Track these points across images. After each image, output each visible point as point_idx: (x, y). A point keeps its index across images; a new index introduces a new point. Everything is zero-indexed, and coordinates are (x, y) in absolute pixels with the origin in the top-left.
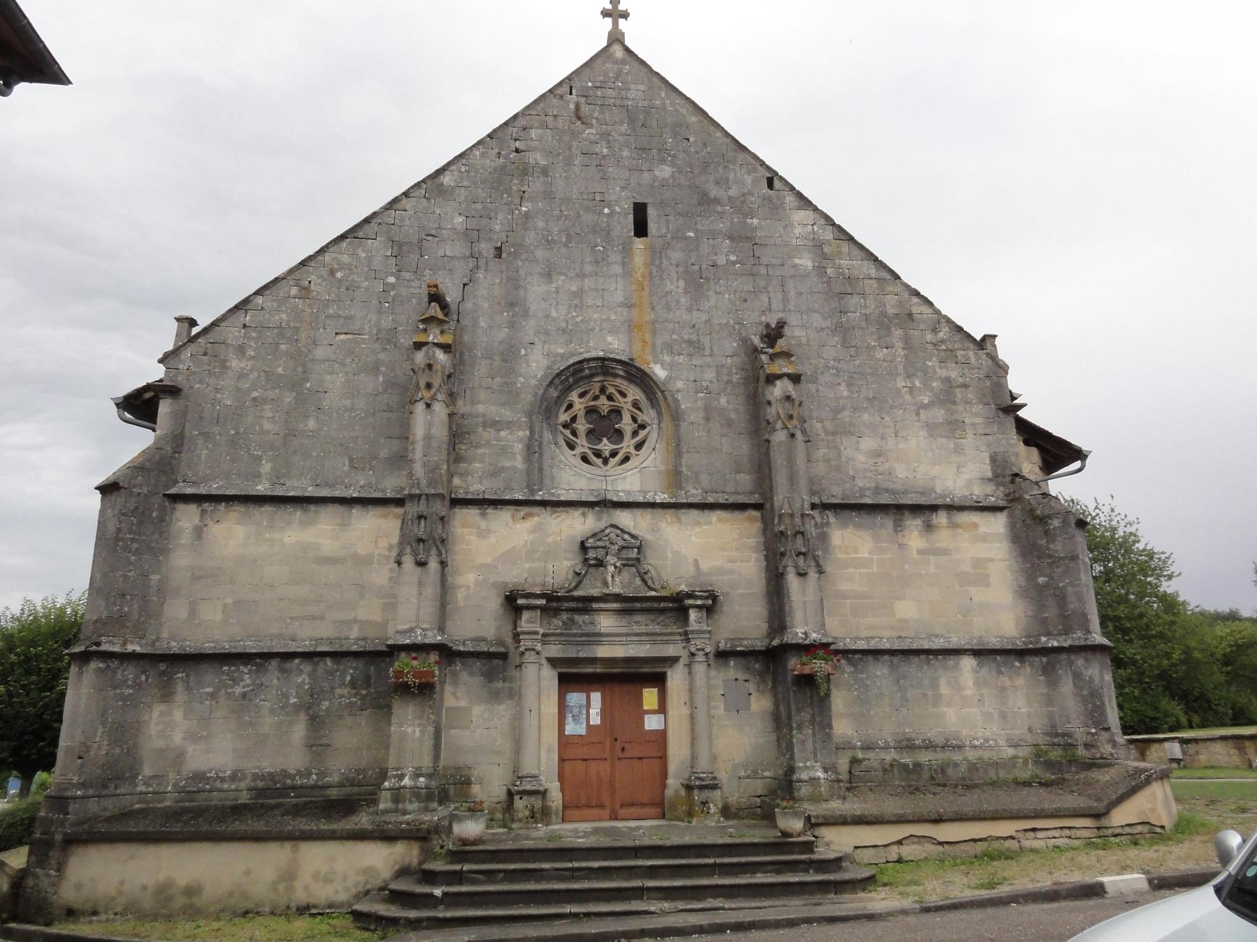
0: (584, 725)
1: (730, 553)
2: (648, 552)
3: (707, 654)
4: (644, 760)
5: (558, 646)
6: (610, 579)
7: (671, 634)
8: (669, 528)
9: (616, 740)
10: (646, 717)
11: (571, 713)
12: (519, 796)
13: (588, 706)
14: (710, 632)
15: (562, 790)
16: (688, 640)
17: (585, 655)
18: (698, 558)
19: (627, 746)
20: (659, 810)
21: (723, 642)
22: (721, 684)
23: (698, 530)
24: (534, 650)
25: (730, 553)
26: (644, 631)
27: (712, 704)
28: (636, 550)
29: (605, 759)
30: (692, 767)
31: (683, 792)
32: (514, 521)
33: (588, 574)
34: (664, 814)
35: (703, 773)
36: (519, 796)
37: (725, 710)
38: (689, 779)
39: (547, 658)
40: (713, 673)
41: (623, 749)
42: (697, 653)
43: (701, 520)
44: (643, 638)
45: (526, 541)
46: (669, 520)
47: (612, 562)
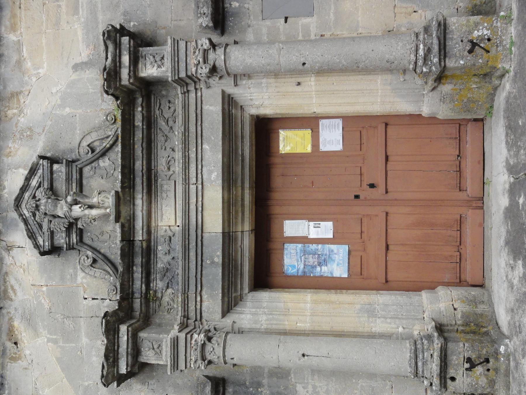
0: (334, 247)
1: (64, 9)
2: (63, 146)
3: (214, 46)
4: (388, 154)
5: (205, 297)
6: (94, 212)
7: (186, 107)
8: (28, 111)
9: (357, 197)
10: (323, 148)
11: (313, 267)
12: (449, 382)
13: (304, 240)
14: (176, 43)
15: (432, 287)
16: (194, 79)
17: (219, 253)
18: (72, 63)
19: (367, 180)
20: (470, 131)
21: (201, 20)
22: (268, 23)
23: (29, 64)
24: (203, 345)
25: (64, 9)
26: (180, 154)
27: (300, 38)
28: (56, 167)
29: (387, 214)
30: (405, 71)
31: (446, 88)
32: (19, 358)
33: (95, 245)
34: (476, 120)
35: (417, 50)
36: (449, 382)
37: (311, 14)
38: (425, 75)
39: (223, 316)
40: (250, 36)
41: (372, 186)
42: (211, 62)
43: (15, 58)
44: (193, 155)
45: (49, 340)
46: (15, 111)
47: (65, 208)
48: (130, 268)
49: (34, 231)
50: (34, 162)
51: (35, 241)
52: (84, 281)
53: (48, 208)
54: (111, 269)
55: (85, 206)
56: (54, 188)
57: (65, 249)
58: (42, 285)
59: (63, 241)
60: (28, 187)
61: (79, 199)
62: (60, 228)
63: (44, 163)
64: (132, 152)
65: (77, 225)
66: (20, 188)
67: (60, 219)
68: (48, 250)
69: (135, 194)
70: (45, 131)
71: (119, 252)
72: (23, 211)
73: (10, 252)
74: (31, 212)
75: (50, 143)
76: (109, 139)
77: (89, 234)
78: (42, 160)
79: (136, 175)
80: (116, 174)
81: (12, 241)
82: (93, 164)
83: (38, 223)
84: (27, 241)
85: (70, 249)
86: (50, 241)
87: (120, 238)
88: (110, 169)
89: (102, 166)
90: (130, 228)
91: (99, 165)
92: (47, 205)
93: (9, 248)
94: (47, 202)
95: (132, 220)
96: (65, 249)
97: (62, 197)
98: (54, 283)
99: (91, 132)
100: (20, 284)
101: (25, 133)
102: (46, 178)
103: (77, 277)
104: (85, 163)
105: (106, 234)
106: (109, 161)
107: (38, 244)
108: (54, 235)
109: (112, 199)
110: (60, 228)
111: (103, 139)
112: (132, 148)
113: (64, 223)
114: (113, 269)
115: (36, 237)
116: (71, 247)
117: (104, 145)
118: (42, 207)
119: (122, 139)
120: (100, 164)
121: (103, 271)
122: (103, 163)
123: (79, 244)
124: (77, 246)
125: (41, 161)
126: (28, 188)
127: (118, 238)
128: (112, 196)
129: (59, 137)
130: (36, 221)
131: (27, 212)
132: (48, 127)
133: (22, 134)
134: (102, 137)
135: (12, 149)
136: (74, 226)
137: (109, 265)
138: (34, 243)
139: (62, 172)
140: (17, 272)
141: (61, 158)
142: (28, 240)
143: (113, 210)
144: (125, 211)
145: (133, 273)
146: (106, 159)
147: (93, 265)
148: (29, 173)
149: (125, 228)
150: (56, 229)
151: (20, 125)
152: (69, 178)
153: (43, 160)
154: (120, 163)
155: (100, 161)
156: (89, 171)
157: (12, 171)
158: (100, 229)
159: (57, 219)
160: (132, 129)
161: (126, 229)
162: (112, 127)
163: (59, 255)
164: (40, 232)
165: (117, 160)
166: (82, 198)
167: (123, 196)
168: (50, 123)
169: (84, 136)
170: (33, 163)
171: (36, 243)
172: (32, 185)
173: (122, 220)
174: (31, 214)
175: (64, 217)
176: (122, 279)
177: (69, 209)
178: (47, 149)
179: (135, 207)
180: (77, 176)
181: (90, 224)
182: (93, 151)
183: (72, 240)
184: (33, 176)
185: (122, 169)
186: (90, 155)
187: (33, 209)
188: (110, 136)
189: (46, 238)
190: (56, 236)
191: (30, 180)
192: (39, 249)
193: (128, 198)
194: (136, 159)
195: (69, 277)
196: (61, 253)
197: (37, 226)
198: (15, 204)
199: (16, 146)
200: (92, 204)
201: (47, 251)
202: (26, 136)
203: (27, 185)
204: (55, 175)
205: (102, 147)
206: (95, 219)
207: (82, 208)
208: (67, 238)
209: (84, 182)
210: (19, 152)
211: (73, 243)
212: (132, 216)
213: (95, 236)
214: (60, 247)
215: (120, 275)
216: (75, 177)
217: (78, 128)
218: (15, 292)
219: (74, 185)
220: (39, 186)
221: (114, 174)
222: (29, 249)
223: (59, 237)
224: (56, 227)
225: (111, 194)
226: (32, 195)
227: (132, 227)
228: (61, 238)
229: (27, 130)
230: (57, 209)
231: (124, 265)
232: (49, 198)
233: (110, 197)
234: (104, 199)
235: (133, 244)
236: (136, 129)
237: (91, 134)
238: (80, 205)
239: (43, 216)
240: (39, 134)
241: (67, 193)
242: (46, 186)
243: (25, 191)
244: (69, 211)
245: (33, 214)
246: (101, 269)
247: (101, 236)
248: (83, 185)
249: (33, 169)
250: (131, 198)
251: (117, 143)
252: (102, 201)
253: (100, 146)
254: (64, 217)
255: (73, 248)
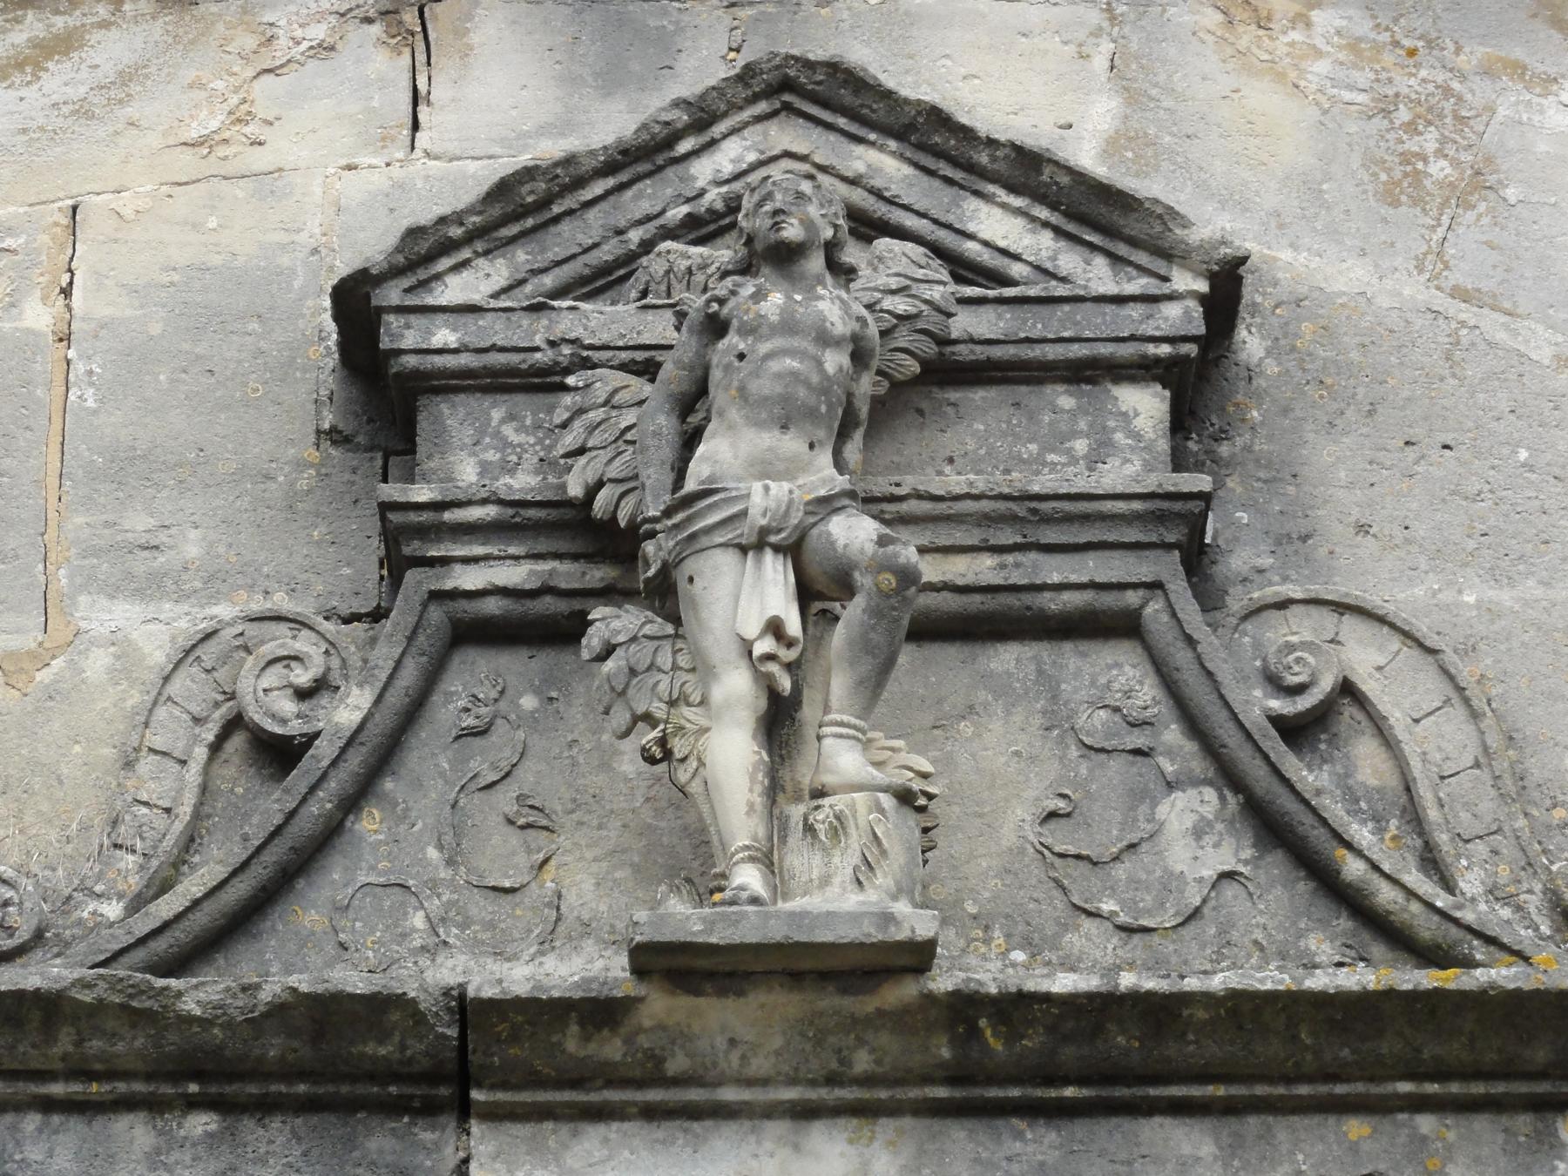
48: (198, 1076)
49: (565, 227)
50: (1186, 224)
51: (469, 239)
52: (98, 663)
53: (764, 348)
54: (196, 903)
55: (789, 667)
56: (954, 395)
57: (392, 491)
58: (67, 292)
59: (467, 473)
60: (958, 175)
61: (853, 612)
62: (581, 451)
63: (1172, 311)
64: (1303, 1090)
65: (608, 594)
66: (947, 106)
67: (665, 451)
68: (385, 343)
69: (907, 1122)
70: (1467, 313)
71: (355, 981)
72: (734, 131)
73: (376, 29)
74: (733, 205)
75: (1354, 355)
76: (1414, 878)
77: (528, 702)
78: (1202, 286)
79: (1080, 1128)
80: (1089, 940)
81: (475, 38)
82: (1172, 733)
83: (630, 258)
84: (472, 166)
85: (392, 537)
86: (464, 360)
87: (489, 992)
88: (1134, 882)
89: (1162, 811)
90: (576, 1084)
91: (1171, 786)
92: (795, 342)
93: (410, 18)
94: (824, 339)
95: (654, 1095)
96: (392, 491)
97: (867, 468)
98: (85, 397)
99: (1475, 715)
100: (83, 111)
101: (1443, 141)
102: (1034, 324)
103: (140, 594)
104: (1181, 657)
105: (522, 860)
106: (1209, 873)
107: (444, 263)
108: (520, 398)
109: (855, 918)
110: (581, 451)
111: (1414, 818)
112: (1340, 1089)
113: (631, 482)
114: (201, 919)
115: (513, 240)
116: (411, 548)
117: (1362, 834)
118: (776, 299)
119: (1415, 997)
120: (1180, 799)
121: (178, 827)
122: (1189, 821)
123: (436, 614)
124: (417, 600)
125: (1187, 281)
126: (948, 171)
127: (496, 968)
128: (888, 919)
129: (1417, 432)
130: (647, 246)
131: (728, 169)
132: (1501, 336)
133: (1427, 115)
134: (1433, 814)
135: (1295, 36)
136: (597, 575)
137: (241, 889)
138: (456, 232)
139: (1094, 460)
140: (197, 85)
141: (1224, 450)
142: (479, 177)
143: (748, 930)
144: (747, 1034)
145: (153, 1106)
146: (1230, 852)
147: (237, 741)
148: (1079, 177)
149: (587, 1039)
150: (581, 411)
151: (1509, 101)
152: (1047, 520)
153: (1203, 299)
154: (1192, 984)
155: (1210, 794)
156: (1115, 698)
157: (1097, 33)
158: (576, 805)
159: (665, 423)
160: (1522, 1088)
161: (572, 1042)
162: (1534, 902)
163: (335, 436)
164: (548, 281)
165: (1223, 952)
166: (862, 645)
167: (880, 1013)
168: (1544, 355)
169: (1432, 652)
170: (1169, 215)
171: (448, 247)
172: (972, 203)
173: (659, 1005)
174: (714, 198)
175: (690, 485)
176: (100, 1006)
177: (764, 532)
178: (1306, 327)
179: (777, 1128)
180: (1067, 596)
181: (620, 717)
182: (1295, 731)
183: (479, 550)
184: (1055, 218)
185: (1137, 998)
186: (1259, 704)
187: (762, 223)
188: (1449, 886)
189: (497, 331)
190: (511, 417)
191: (1012, 189)
192: (394, 272)
193: (862, 1062)
194: (1233, 1123)
195: (138, 523)
196: (353, 459)
197: (607, 253)
198: (810, 65)
199: (1322, 67)
200: (810, 732)
201: (375, 338)
202: (1412, 145)
203: (971, 168)
204: (1064, 399)
205: (1334, 810)
206: (668, 755)
207: (764, 646)
208: (489, 512)
209: (1008, 658)
210: (1263, 98)
211: (445, 561)
212: (694, 1095)
213: (507, 756)
214: (411, 449)
215: (141, 991)
216: (1056, 578)
217: (1505, 597)
218: (20, 66)
219: (983, 569)
220: (962, 269)
221: (1088, 924)
222: (400, 186)
223: (505, 444)
224: (595, 415)
225: (902, 908)
226: (881, 210)
227: (593, 1097)
228: (492, 456)
229: (1466, 157)
230: (759, 425)
231: (229, 1025)
232: (859, 356)
233: (872, 897)
234: (855, 841)
235: (428, 1110)
236: (1523, 1122)
237: (1458, 712)
238: (794, 626)
239: (695, 302)
240: (1434, 261)
241: (905, 507)
242: (966, 323)
243: (921, 147)
244: (745, 532)
245: (714, 215)
246: (197, 815)
247: (511, 809)
248: (978, 649)
249: (1117, 218)
250: (867, 1081)
251: (1378, 950)
252: (839, 827)
253: (1351, 798)
254: (690, 485)
255: (395, 566)
